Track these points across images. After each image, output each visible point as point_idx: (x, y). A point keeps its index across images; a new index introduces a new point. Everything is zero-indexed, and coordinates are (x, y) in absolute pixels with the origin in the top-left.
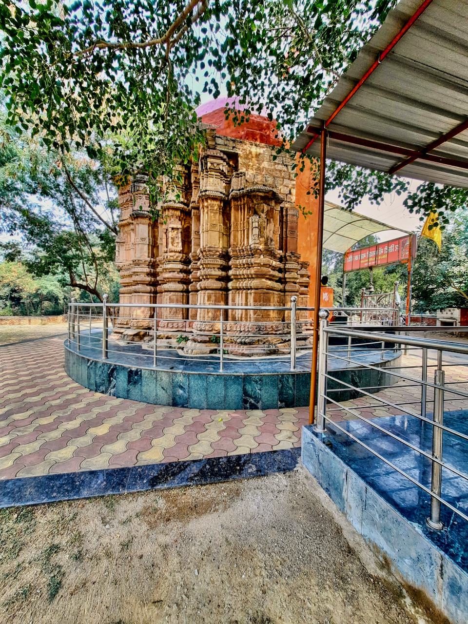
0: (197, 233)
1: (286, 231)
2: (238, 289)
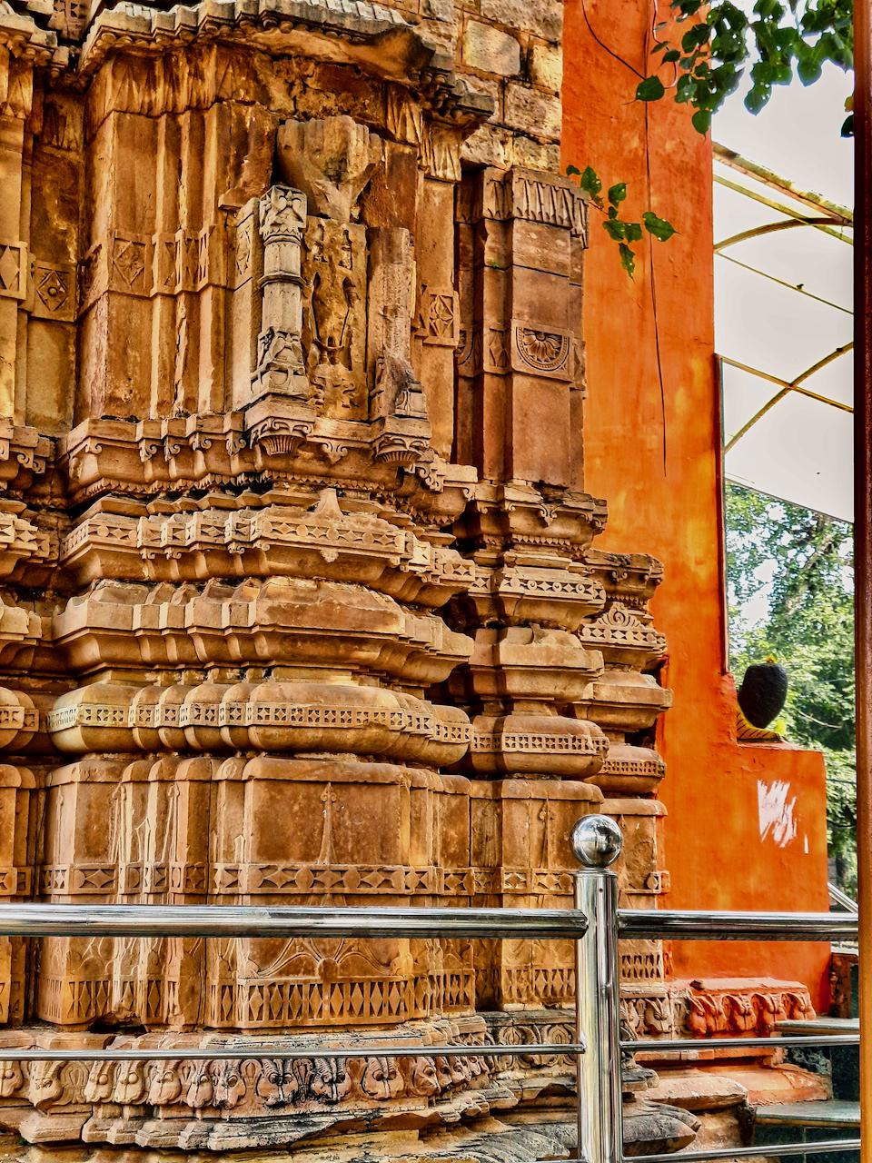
1: (504, 332)
2: (135, 752)
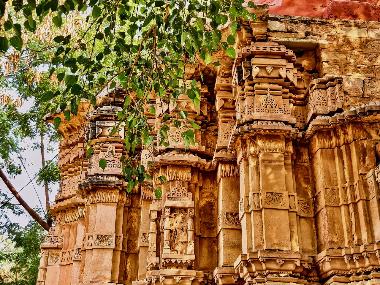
0: (234, 216)
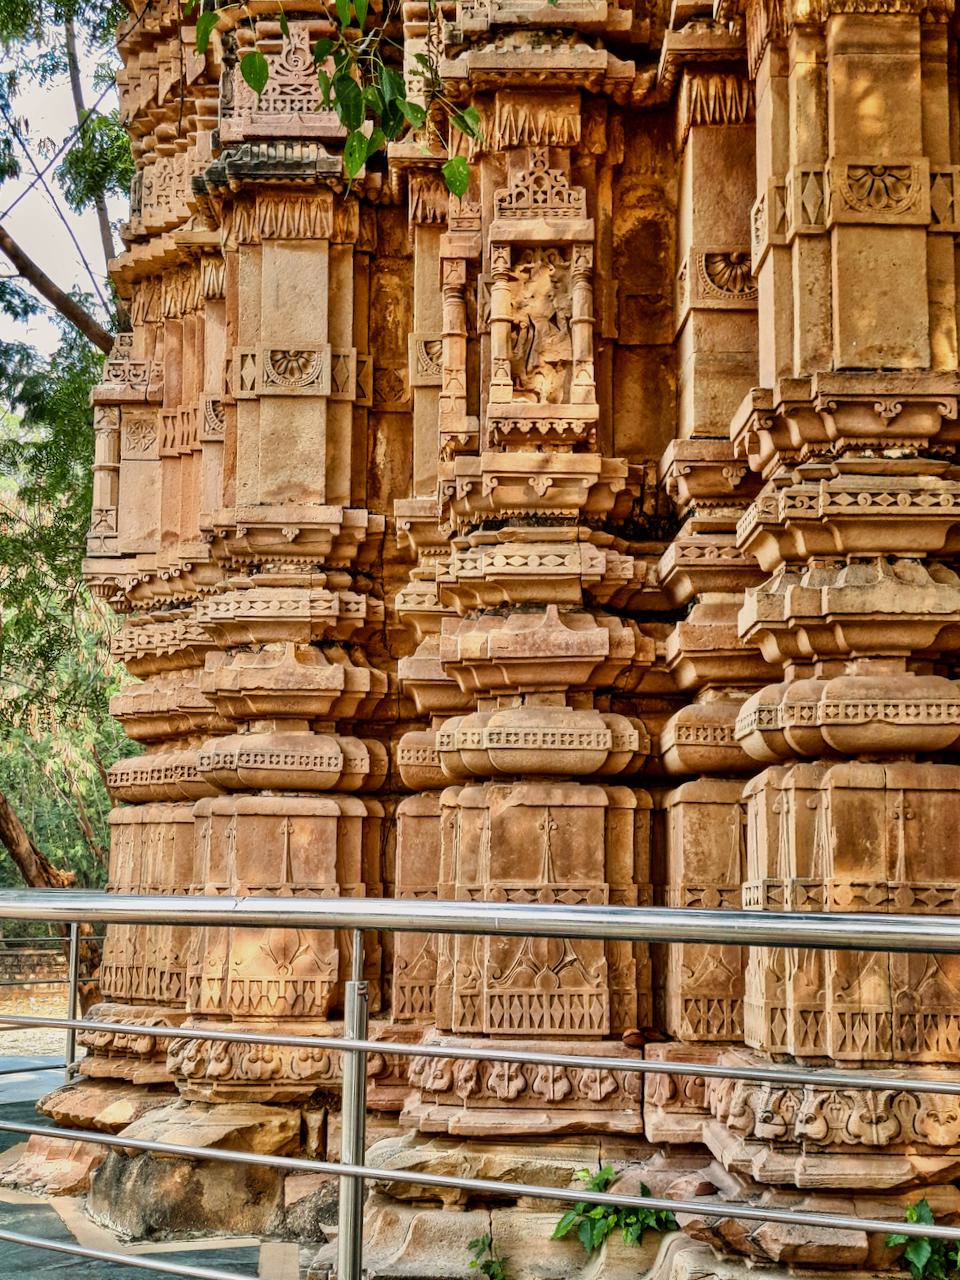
0: (732, 266)
